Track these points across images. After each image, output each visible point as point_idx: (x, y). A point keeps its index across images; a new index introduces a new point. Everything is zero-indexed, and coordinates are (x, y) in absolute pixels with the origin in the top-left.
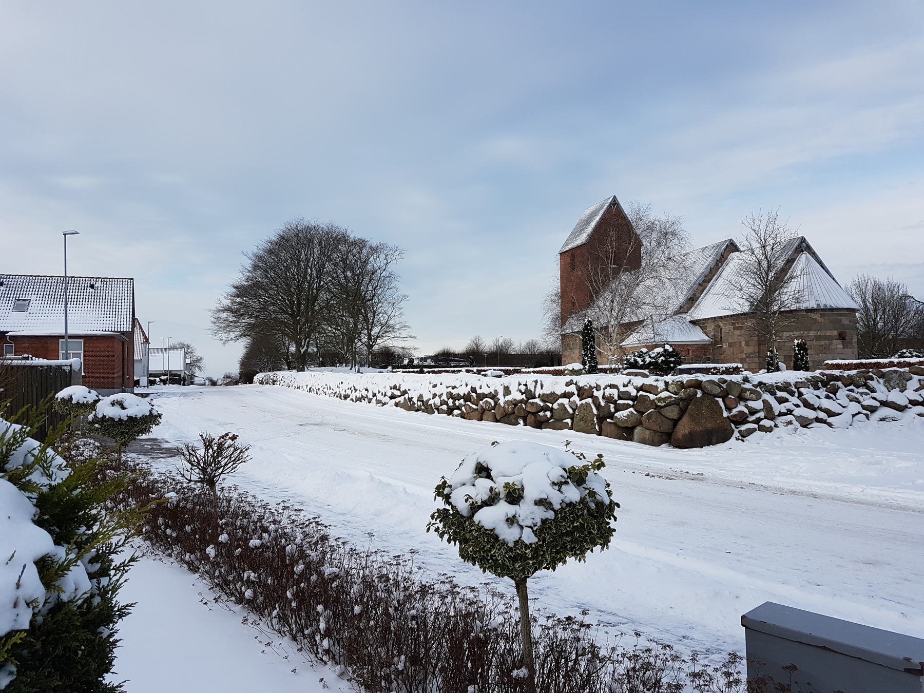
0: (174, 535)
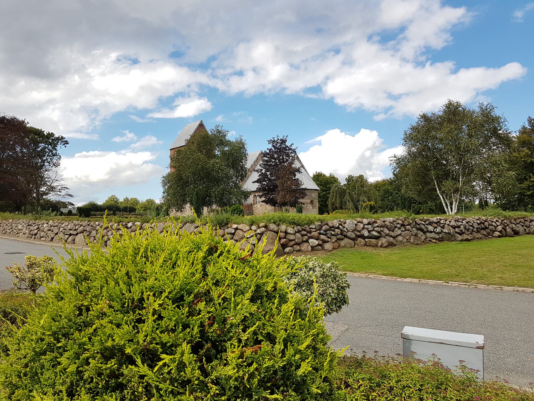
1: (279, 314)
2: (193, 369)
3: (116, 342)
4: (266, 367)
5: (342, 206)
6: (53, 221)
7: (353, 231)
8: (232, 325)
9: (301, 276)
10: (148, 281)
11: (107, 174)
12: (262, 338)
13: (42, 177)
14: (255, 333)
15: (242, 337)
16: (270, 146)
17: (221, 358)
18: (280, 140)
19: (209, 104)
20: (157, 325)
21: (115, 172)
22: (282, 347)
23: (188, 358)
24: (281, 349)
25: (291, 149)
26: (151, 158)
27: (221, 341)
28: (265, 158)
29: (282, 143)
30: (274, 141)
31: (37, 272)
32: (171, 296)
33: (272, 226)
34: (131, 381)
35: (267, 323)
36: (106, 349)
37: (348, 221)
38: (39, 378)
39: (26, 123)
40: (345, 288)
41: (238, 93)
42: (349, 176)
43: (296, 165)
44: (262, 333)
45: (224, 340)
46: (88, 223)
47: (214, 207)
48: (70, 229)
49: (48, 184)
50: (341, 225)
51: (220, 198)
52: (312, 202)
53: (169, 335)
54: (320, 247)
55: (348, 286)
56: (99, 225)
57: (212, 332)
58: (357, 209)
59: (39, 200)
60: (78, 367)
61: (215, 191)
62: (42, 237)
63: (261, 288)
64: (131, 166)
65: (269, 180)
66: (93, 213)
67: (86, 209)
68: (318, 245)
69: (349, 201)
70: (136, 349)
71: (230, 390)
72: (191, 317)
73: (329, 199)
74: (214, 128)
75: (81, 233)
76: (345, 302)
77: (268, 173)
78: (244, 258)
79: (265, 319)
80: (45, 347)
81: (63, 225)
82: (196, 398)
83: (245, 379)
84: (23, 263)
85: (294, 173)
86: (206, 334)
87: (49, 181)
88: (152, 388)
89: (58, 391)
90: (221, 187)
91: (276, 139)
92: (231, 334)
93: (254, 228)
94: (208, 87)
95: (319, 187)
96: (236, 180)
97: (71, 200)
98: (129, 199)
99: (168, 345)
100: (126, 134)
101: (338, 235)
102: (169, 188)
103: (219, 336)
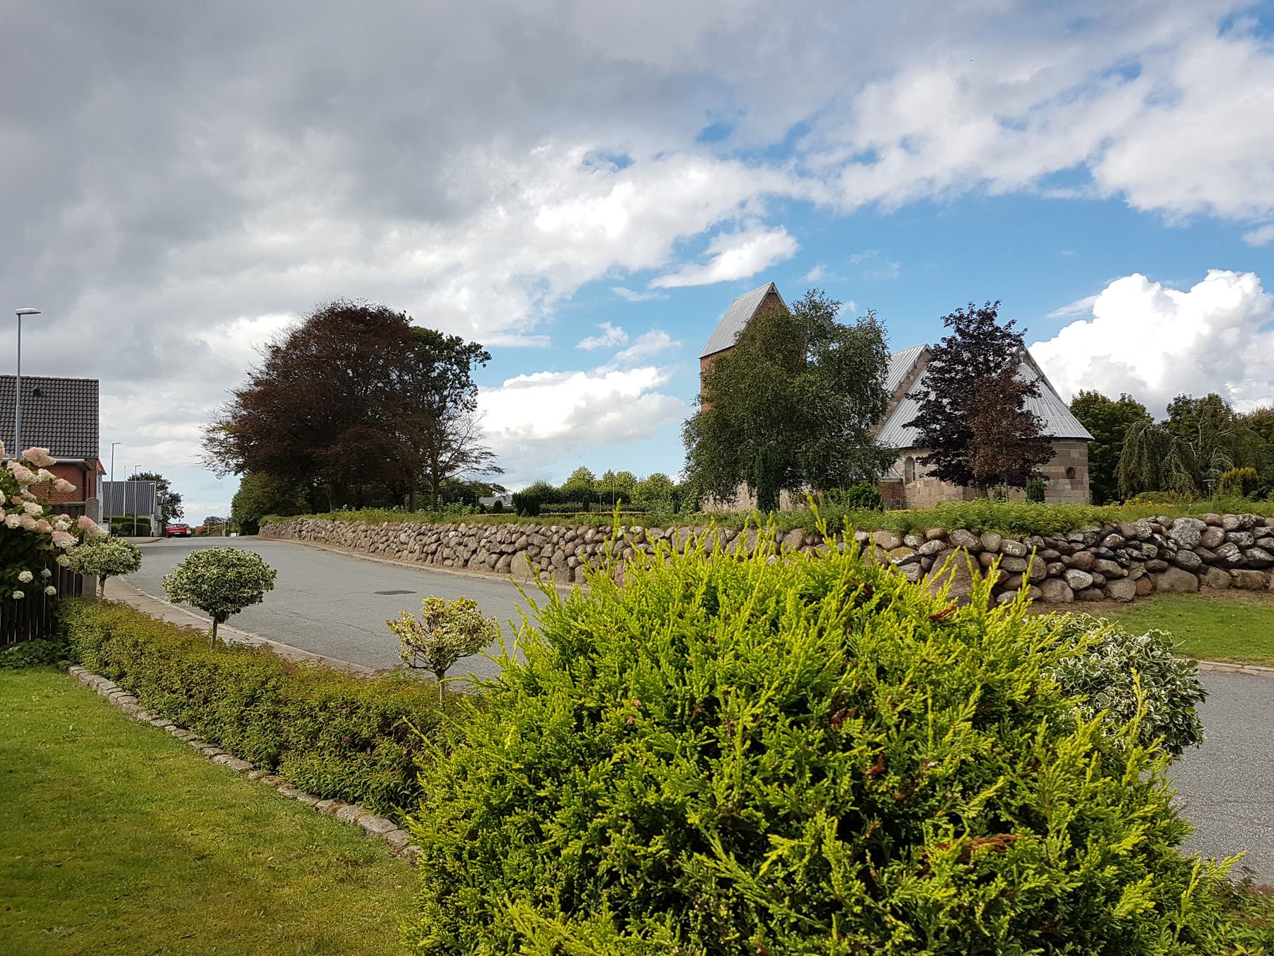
0: (871, 796)
1: (1051, 763)
2: (846, 878)
3: (664, 796)
4: (1029, 889)
5: (1157, 483)
6: (467, 525)
7: (1194, 549)
8: (933, 781)
9: (1066, 668)
10: (720, 658)
11: (566, 422)
12: (1010, 818)
13: (442, 433)
14: (990, 804)
15: (964, 811)
16: (950, 332)
17: (909, 857)
18: (979, 315)
19: (790, 241)
20: (753, 764)
21: (584, 416)
22: (1068, 844)
23: (833, 848)
24: (1064, 849)
25: (1009, 335)
26: (657, 380)
27: (905, 815)
28: (937, 364)
29: (982, 322)
30: (961, 317)
31: (446, 633)
32: (779, 699)
33: (961, 536)
34: (699, 890)
35: (1020, 782)
36: (642, 810)
37: (1179, 522)
38: (499, 865)
39: (407, 319)
40: (1194, 701)
41: (862, 207)
42: (1177, 400)
43: (1024, 375)
44: (1007, 805)
45: (915, 816)
46: (536, 529)
47: (806, 489)
48: (500, 542)
49: (454, 446)
50: (1160, 532)
51: (819, 468)
52: (1070, 473)
53: (782, 790)
54: (1098, 592)
55: (1201, 695)
56: (557, 532)
57: (883, 793)
58: (1202, 488)
59: (436, 482)
60: (585, 848)
61: (808, 450)
62: (446, 558)
63: (997, 695)
64: (618, 402)
65: (949, 418)
66: (543, 506)
67: (531, 498)
68: (1094, 585)
69: (1177, 467)
70: (710, 816)
71: (936, 936)
72: (830, 753)
73: (1121, 464)
74: (803, 299)
75: (521, 550)
76: (1193, 738)
77: (945, 401)
78: (939, 616)
79: (1014, 771)
80: (509, 797)
81: (487, 533)
82: (855, 946)
83: (978, 915)
84: (420, 614)
85: (1018, 396)
86: (867, 795)
87: (455, 441)
88: (748, 911)
89: (541, 897)
90: (821, 441)
91: (966, 312)
92: (933, 802)
93: (911, 540)
94: (787, 201)
95: (1089, 431)
96: (860, 423)
97: (492, 479)
98: (615, 474)
99: (781, 813)
100: (605, 329)
101: (1152, 559)
102: (699, 447)
103: (899, 803)
